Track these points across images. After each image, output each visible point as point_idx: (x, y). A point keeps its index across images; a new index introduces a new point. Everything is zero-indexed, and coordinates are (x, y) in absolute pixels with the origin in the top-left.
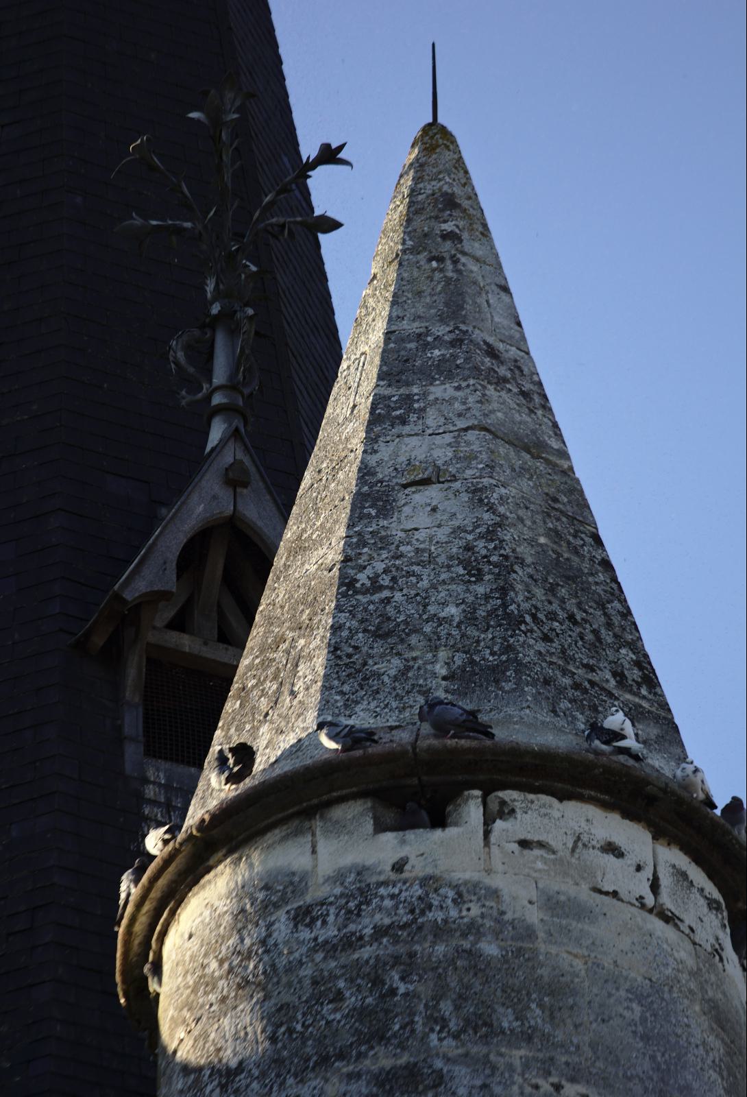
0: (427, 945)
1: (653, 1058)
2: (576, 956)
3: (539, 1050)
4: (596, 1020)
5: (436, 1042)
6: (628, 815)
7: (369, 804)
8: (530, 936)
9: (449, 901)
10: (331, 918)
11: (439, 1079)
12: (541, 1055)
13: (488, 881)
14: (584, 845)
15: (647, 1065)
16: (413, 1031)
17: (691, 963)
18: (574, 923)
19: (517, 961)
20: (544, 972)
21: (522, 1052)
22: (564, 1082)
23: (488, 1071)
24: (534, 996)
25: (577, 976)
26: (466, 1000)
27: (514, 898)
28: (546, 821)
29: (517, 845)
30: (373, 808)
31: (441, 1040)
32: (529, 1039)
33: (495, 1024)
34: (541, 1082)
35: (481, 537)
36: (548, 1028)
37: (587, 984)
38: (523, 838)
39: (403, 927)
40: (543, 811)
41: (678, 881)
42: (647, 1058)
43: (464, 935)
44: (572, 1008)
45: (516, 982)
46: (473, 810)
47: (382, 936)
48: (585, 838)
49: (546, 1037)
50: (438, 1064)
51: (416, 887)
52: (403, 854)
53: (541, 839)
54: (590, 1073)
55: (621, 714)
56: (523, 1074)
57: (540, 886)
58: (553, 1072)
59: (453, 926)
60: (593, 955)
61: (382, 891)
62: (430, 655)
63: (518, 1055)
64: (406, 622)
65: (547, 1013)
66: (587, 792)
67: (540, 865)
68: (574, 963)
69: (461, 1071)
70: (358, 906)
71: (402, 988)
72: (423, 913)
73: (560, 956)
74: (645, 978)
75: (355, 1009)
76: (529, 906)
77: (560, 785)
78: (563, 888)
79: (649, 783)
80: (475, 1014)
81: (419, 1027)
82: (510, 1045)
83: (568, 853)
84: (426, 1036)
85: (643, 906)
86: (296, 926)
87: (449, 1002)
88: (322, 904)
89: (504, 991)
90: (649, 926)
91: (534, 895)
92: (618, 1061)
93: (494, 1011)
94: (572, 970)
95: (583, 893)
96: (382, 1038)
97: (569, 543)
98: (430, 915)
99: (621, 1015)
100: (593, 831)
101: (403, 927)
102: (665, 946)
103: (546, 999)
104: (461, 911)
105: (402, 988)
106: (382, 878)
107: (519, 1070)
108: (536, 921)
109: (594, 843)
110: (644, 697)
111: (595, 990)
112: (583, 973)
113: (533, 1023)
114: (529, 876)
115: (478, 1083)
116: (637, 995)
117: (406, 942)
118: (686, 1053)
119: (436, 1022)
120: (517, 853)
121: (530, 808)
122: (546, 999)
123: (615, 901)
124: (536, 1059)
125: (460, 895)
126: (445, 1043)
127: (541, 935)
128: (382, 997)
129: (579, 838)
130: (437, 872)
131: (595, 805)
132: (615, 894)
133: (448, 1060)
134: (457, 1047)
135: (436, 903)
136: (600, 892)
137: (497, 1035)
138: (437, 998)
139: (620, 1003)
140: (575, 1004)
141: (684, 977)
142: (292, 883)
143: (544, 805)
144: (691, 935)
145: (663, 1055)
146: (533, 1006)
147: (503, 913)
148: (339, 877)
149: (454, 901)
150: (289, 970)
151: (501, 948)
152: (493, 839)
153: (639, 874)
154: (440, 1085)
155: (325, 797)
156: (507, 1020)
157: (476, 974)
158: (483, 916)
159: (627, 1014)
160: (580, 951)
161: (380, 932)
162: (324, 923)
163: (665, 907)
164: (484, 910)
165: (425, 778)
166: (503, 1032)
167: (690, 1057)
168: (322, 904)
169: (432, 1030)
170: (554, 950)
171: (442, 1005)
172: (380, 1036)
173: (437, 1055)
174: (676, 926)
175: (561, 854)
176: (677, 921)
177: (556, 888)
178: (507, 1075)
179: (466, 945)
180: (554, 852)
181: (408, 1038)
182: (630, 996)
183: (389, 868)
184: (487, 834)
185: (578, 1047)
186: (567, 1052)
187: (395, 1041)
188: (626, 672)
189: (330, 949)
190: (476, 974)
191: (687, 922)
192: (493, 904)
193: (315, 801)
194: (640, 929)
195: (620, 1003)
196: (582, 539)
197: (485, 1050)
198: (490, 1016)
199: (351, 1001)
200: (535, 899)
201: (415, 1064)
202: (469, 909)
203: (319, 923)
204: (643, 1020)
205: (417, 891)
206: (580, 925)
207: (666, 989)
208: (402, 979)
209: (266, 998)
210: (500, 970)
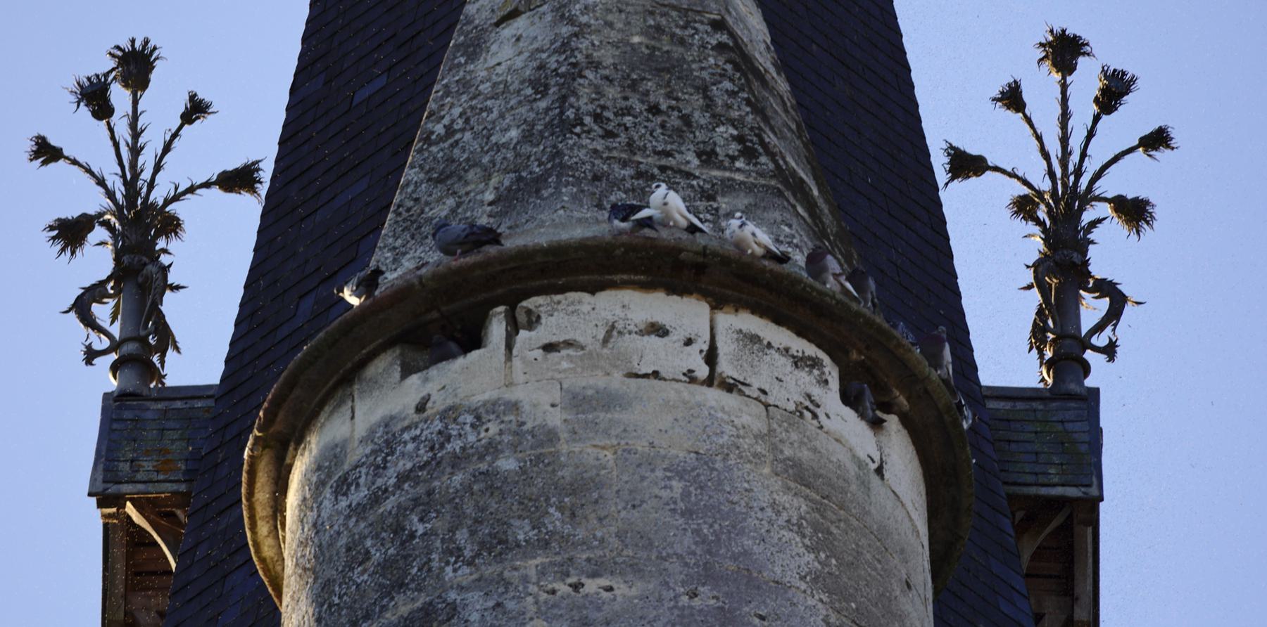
0: (445, 478)
1: (697, 532)
2: (603, 448)
3: (556, 554)
4: (625, 508)
5: (451, 574)
6: (672, 290)
7: (398, 352)
8: (551, 440)
9: (468, 428)
10: (362, 481)
11: (453, 609)
12: (558, 558)
13: (510, 395)
14: (620, 333)
15: (688, 540)
16: (430, 570)
17: (759, 425)
18: (602, 415)
19: (535, 469)
20: (566, 473)
21: (538, 561)
22: (584, 580)
23: (501, 590)
24: (554, 499)
25: (604, 468)
26: (481, 523)
27: (535, 406)
28: (574, 318)
29: (541, 351)
30: (402, 354)
31: (455, 571)
32: (547, 544)
33: (510, 539)
34: (556, 586)
35: (555, 51)
36: (567, 529)
37: (615, 473)
38: (547, 341)
39: (421, 468)
40: (571, 308)
41: (745, 346)
42: (689, 533)
43: (481, 458)
44: (596, 502)
45: (535, 490)
46: (497, 329)
47: (405, 482)
48: (620, 326)
49: (565, 539)
50: (452, 595)
51: (437, 422)
52: (424, 393)
53: (567, 337)
54: (615, 563)
55: (664, 186)
56: (537, 583)
57: (565, 386)
58: (572, 571)
59: (471, 451)
60: (623, 442)
61: (406, 436)
62: (482, 186)
63: (532, 565)
64: (468, 160)
65: (567, 513)
66: (617, 278)
67: (565, 365)
68: (601, 456)
69: (475, 597)
70: (385, 461)
71: (421, 529)
72: (442, 446)
73: (588, 452)
74: (690, 452)
75: (379, 564)
76: (551, 409)
77: (586, 277)
78: (592, 381)
79: (681, 250)
80: (490, 534)
81: (435, 564)
82: (526, 556)
83: (598, 346)
84: (442, 569)
85: (693, 380)
86: (336, 499)
87: (465, 530)
88: (357, 467)
89: (521, 503)
90: (698, 398)
91: (557, 396)
92: (651, 544)
93: (510, 526)
94: (597, 463)
95: (617, 381)
96: (401, 586)
97: (673, 35)
98: (449, 447)
99: (656, 497)
100: (629, 316)
101: (421, 468)
102: (720, 415)
103: (566, 500)
104: (479, 433)
105: (421, 529)
106: (406, 423)
107: (534, 580)
108: (558, 423)
109: (632, 328)
110: (738, 170)
111: (625, 478)
112: (611, 463)
113: (550, 528)
114: (552, 379)
115: (491, 603)
116: (679, 472)
117: (425, 481)
118: (745, 520)
119: (451, 554)
120: (540, 359)
121: (557, 310)
122: (566, 500)
123: (656, 381)
124: (552, 564)
125: (478, 418)
126: (460, 572)
127: (564, 436)
128: (403, 543)
129: (613, 327)
130: (457, 401)
131: (634, 289)
132: (656, 374)
133: (461, 588)
134: (471, 574)
135: (454, 433)
136: (637, 376)
137: (511, 550)
138: (453, 530)
139: (656, 483)
140: (601, 497)
141: (745, 443)
142: (335, 456)
143: (573, 303)
144: (763, 398)
145: (711, 526)
146: (552, 510)
147: (523, 423)
148: (369, 437)
149: (473, 426)
150: (330, 545)
151: (519, 460)
152: (515, 352)
153: (688, 348)
154: (453, 617)
155: (357, 358)
156: (522, 531)
157: (492, 494)
158: (501, 433)
159: (665, 494)
160: (608, 442)
161: (403, 478)
162: (358, 485)
163: (724, 375)
164: (502, 426)
165: (444, 309)
166: (518, 546)
167: (751, 522)
168: (357, 467)
169: (448, 563)
170: (577, 448)
171: (458, 536)
172: (400, 586)
173: (452, 587)
174: (741, 393)
175: (589, 348)
176: (740, 386)
177: (584, 384)
178: (521, 588)
179: (483, 467)
180: (583, 348)
181: (424, 579)
182: (668, 474)
183: (412, 411)
184: (509, 346)
185: (602, 540)
186: (590, 548)
187: (413, 586)
188: (718, 149)
189: (358, 511)
190: (492, 494)
191: (756, 385)
192: (512, 418)
193: (349, 365)
194: (685, 403)
195: (656, 483)
196: (695, 28)
197: (499, 568)
198: (505, 532)
199: (377, 556)
200: (558, 401)
201: (431, 603)
202: (487, 430)
203: (353, 488)
204: (686, 495)
205: (438, 425)
206: (609, 416)
207: (719, 458)
208: (421, 520)
209: (316, 579)
210: (517, 482)
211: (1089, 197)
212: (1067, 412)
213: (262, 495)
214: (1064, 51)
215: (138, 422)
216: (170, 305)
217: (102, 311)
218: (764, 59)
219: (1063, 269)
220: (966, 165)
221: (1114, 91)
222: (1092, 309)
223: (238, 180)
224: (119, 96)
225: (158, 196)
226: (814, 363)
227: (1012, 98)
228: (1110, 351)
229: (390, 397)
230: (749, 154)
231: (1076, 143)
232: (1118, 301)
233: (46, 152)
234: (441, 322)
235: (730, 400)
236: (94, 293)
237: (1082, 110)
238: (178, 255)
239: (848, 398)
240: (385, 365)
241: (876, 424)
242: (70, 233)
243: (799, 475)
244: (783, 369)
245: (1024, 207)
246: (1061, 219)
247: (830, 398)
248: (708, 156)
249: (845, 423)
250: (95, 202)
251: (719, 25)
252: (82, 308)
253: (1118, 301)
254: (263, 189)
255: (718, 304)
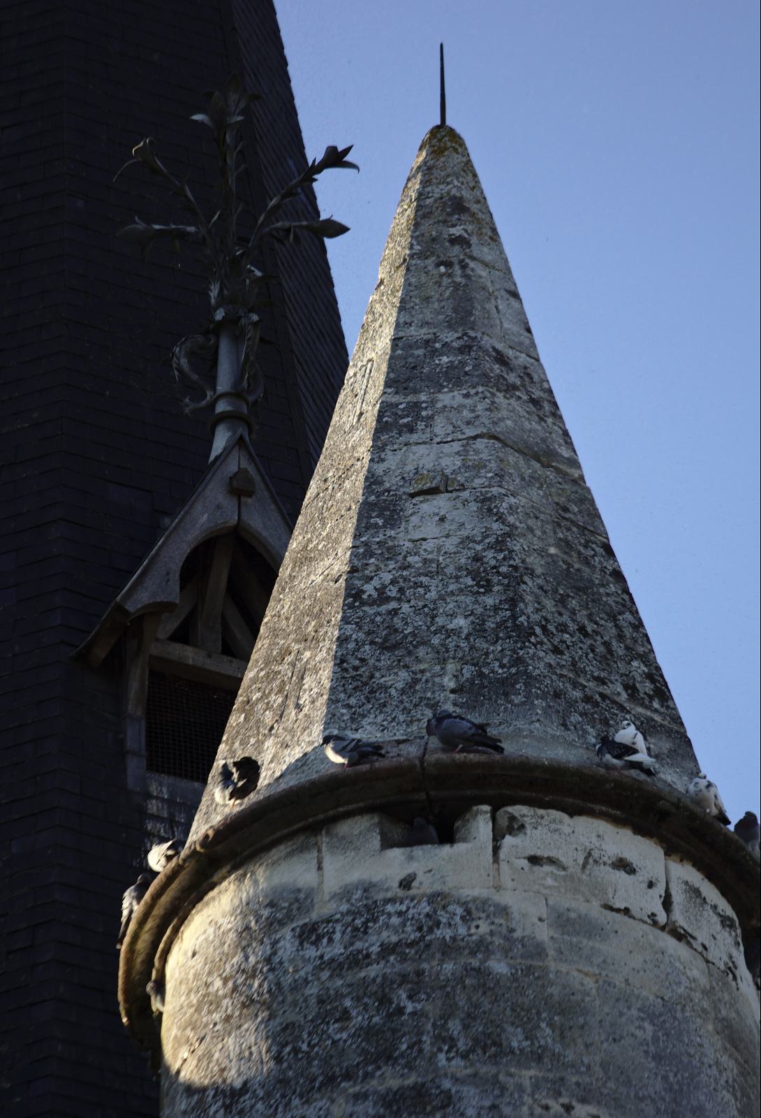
0: (435, 963)
1: (665, 1078)
2: (587, 974)
3: (550, 1070)
4: (607, 1040)
5: (444, 1062)
6: (640, 830)
7: (376, 820)
8: (539, 954)
9: (458, 919)
10: (337, 936)
11: (447, 1100)
12: (551, 1076)
13: (497, 898)
14: (595, 861)
15: (659, 1085)
16: (421, 1051)
17: (704, 981)
18: (585, 941)
19: (526, 979)
20: (554, 990)
21: (532, 1072)
22: (574, 1103)
23: (497, 1092)
24: (544, 1015)
25: (588, 995)
26: (474, 1019)
27: (524, 916)
28: (556, 836)
29: (526, 861)
30: (380, 823)
31: (449, 1060)
32: (539, 1059)
33: (505, 1044)
34: (551, 1102)
35: (490, 547)
36: (558, 1048)
37: (598, 1003)
38: (533, 854)
39: (411, 945)
40: (553, 826)
41: (691, 898)
42: (659, 1079)
43: (473, 953)
44: (582, 1027)
45: (526, 1000)
46: (482, 826)
47: (390, 954)
48: (596, 854)
49: (556, 1057)
50: (447, 1084)
51: (424, 904)
52: (410, 871)
53: (551, 855)
54: (601, 1094)
55: (632, 727)
56: (532, 1095)
57: (550, 902)
58: (564, 1092)
59: (462, 944)
60: (604, 973)
61: (389, 908)
62: (438, 668)
63: (528, 1075)
64: (413, 634)
65: (557, 1032)
66: (598, 807)
67: (550, 881)
68: (585, 982)
70: (365, 924)
71: (410, 1007)
72: (431, 930)
73: (571, 974)
74: (657, 997)
75: (361, 1028)
76: (539, 923)
77: (570, 800)
78: (574, 905)
79: (661, 798)
80: (484, 1033)
81: (427, 1047)
82: (519, 1065)
83: (579, 870)
84: (434, 1055)
85: (655, 923)
86: (301, 944)
87: (457, 1021)
88: (328, 921)
89: (513, 1010)
90: (661, 944)
91: (544, 912)
92: (630, 1081)
93: (504, 1030)
94: (582, 988)
95: (594, 910)
96: (389, 1058)
97: (579, 553)
98: (438, 933)
99: (632, 1035)
100: (604, 847)
101: (411, 945)
102: (677, 964)
103: (556, 1018)
104: (469, 928)
105: (410, 1007)
106: (389, 895)
107: (529, 1090)
108: (546, 939)
109: (605, 859)
110: (656, 711)
111: (606, 1009)
112: (594, 991)
113: (543, 1042)
114: (538, 892)
115: (487, 1103)
116: (649, 1014)
117: (414, 960)
118: (699, 1074)
119: (444, 1042)
120: (526, 869)
121: (540, 824)
122: (556, 1018)
123: (626, 918)
124: (546, 1079)
125: (468, 912)
126: (453, 1062)
127: (551, 953)
128: (390, 1016)
129: (590, 854)
130: (446, 889)
131: (607, 821)
132: (626, 911)
133: (456, 1080)
134: (466, 1067)
135: (444, 920)
136: (611, 909)
137: (506, 1055)
138: (446, 1017)
139: (632, 1022)
140: (586, 1023)
141: (697, 996)
142: (297, 900)
143: (554, 821)
144: (704, 953)
145: (675, 1075)
146: (543, 1025)
147: (512, 930)
148: (345, 894)
149: (462, 918)
150: (294, 988)
151: (511, 967)
152: (502, 855)
153: (651, 891)
155: (331, 813)
156: (516, 1039)
157: (485, 993)
158: (492, 933)
159: (639, 1033)
160: (591, 969)
161: (387, 950)
162: (331, 940)
163: (677, 924)
164: (493, 927)
165: (433, 793)
166: (512, 1052)
167: (703, 1078)
168: (328, 921)
169: (440, 1050)
170: (564, 968)
171: (450, 1024)
172: (387, 1056)
173: (446, 1075)
174: (689, 943)
175: (571, 870)
176: (689, 938)
177: (567, 905)
178: (516, 1096)
179: (475, 963)
180: (564, 869)
181: (415, 1058)
182: (642, 1015)
183: (396, 884)
184: (496, 850)
185: (589, 1067)
186: (578, 1072)
187: (402, 1061)
188: (638, 685)
189: (336, 967)
190: (485, 993)
191: (700, 940)
192: (502, 921)
193: (321, 817)
194: (652, 946)
195: (632, 1022)
196: (593, 550)
197: (494, 1070)
198: (499, 1035)
199: (358, 1020)
200: (545, 916)
201: (423, 1085)
202: (477, 927)
203: (325, 941)
204: (656, 1039)
205: (425, 908)
206: (590, 943)
207: (679, 1008)
208: (410, 997)
209: (271, 1017)
210: (509, 988)
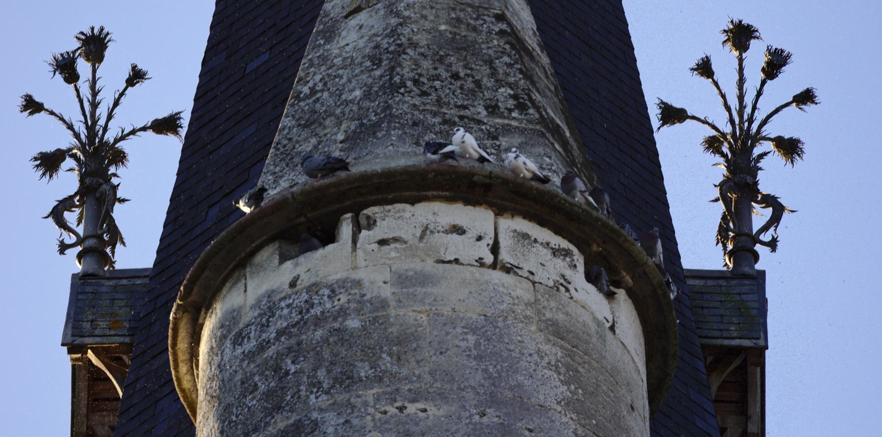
0: (310, 333)
1: (485, 371)
2: (420, 312)
3: (387, 386)
4: (435, 354)
5: (314, 400)
6: (468, 202)
7: (277, 245)
8: (383, 307)
9: (325, 298)
10: (252, 335)
11: (316, 424)
12: (389, 389)
13: (355, 276)
14: (432, 232)
15: (479, 376)
16: (299, 397)
17: (528, 296)
18: (419, 289)
19: (373, 327)
20: (394, 330)
21: (375, 391)
22: (406, 404)
23: (349, 411)
24: (385, 348)
25: (421, 326)
26: (335, 364)
27: (372, 283)
28: (400, 222)
29: (376, 245)
30: (280, 247)
31: (317, 398)
32: (380, 379)
33: (355, 375)
34: (387, 408)
35: (387, 36)
36: (395, 369)
37: (428, 330)
38: (381, 238)
39: (293, 326)
40: (397, 215)
41: (519, 241)
42: (480, 372)
43: (335, 319)
44: (415, 350)
45: (372, 341)
46: (346, 229)
47: (282, 336)
48: (431, 227)
49: (393, 375)
50: (315, 415)
51: (304, 294)
52: (295, 274)
53: (395, 235)
54: (428, 392)
55: (462, 129)
56: (374, 407)
57: (393, 269)
58: (398, 398)
59: (328, 314)
60: (434, 308)
61: (283, 304)
62: (335, 130)
63: (370, 394)
64: (326, 111)
65: (395, 358)
66: (430, 194)
67: (393, 254)
68: (418, 318)
69: (330, 416)
70: (268, 321)
71: (293, 369)
72: (308, 311)
73: (410, 315)
74: (480, 315)
75: (264, 393)
76: (384, 285)
77: (408, 193)
78: (412, 266)
79: (474, 175)
80: (341, 372)
81: (303, 393)
82: (366, 388)
83: (416, 241)
84: (308, 397)
85: (482, 265)
86: (234, 348)
87: (324, 370)
88: (248, 325)
89: (362, 351)
90: (486, 277)
91: (388, 276)
92: (453, 379)
93: (355, 366)
94: (416, 323)
95: (429, 266)
96: (279, 408)
97: (469, 25)
98: (312, 311)
99: (457, 346)
100: (438, 220)
101: (293, 326)
102: (501, 289)
103: (394, 348)
104: (333, 302)
105: (293, 369)
106: (283, 295)
107: (372, 404)
108: (389, 295)
109: (440, 228)
110: (514, 118)
111: (435, 333)
112: (426, 323)
113: (383, 368)
114: (385, 264)
115: (342, 421)
116: (473, 329)
117: (296, 335)
118: (518, 362)
119: (314, 386)
120: (376, 250)
121: (388, 216)
122: (394, 348)
123: (457, 266)
124: (385, 393)
125: (333, 291)
126: (320, 399)
127: (393, 304)
128: (280, 379)
129: (427, 228)
130: (318, 279)
131: (441, 201)
132: (456, 261)
133: (321, 410)
134: (328, 400)
135: (316, 302)
136: (443, 262)
137: (356, 383)
138: (315, 370)
139: (457, 337)
140: (418, 346)
141: (519, 309)
142: (233, 318)
143: (399, 211)
144: (531, 277)
145: (495, 367)
146: (384, 356)
147: (364, 295)
148: (257, 305)
149: (329, 297)
150: (230, 380)
151: (361, 321)
152: (358, 245)
153: (479, 243)
154: (315, 430)
155: (248, 250)
156: (364, 370)
157: (343, 344)
158: (349, 302)
159: (463, 344)
160: (423, 308)
161: (280, 333)
162: (249, 338)
163: (504, 261)
164: (350, 297)
165: (309, 215)
166: (361, 380)
167: (523, 364)
168: (248, 325)
169: (312, 393)
170: (401, 312)
171: (319, 373)
172: (279, 408)
173: (314, 409)
174: (516, 274)
175: (410, 242)
176: (515, 269)
177: (406, 268)
178: (362, 410)
179: (336, 325)
180: (406, 243)
181: (295, 404)
182: (465, 330)
183: (287, 286)
184: (355, 241)
185: (419, 377)
186: (411, 382)
187: (287, 408)
188: (500, 104)
189: (250, 356)
190: (343, 344)
191: (526, 268)
192: (357, 291)
193: (243, 254)
194: (477, 281)
195: (457, 337)
196: (484, 20)
197: (347, 396)
198: (352, 371)
199: (262, 388)
200: (388, 279)
201: (300, 420)
202: (339, 300)
203: (246, 340)
204: (477, 345)
205: (305, 296)
206: (424, 290)
207: (500, 319)
208: (293, 362)
209: (220, 404)
210: (360, 336)
211: (758, 137)
212: (743, 287)
213: (183, 345)
214: (741, 36)
215: (96, 294)
216: (119, 212)
217: (71, 217)
218: (532, 41)
219: (740, 187)
220: (672, 115)
221: (776, 63)
222: (760, 215)
223: (165, 125)
224: (83, 67)
225: (110, 137)
226: (567, 253)
227: (705, 68)
228: (773, 244)
229: (272, 277)
230: (521, 107)
231: (749, 100)
232: (778, 210)
233: (32, 106)
234: (307, 225)
235: (508, 279)
236: (65, 204)
237: (753, 76)
238: (124, 178)
239: (591, 278)
240: (268, 254)
241: (610, 296)
242: (49, 162)
243: (556, 331)
244: (545, 257)
245: (713, 144)
246: (739, 153)
247: (578, 277)
248: (493, 109)
249: (588, 295)
250: (66, 141)
251: (501, 18)
252: (57, 214)
253: (778, 210)
254: (183, 132)
255: (500, 212)
